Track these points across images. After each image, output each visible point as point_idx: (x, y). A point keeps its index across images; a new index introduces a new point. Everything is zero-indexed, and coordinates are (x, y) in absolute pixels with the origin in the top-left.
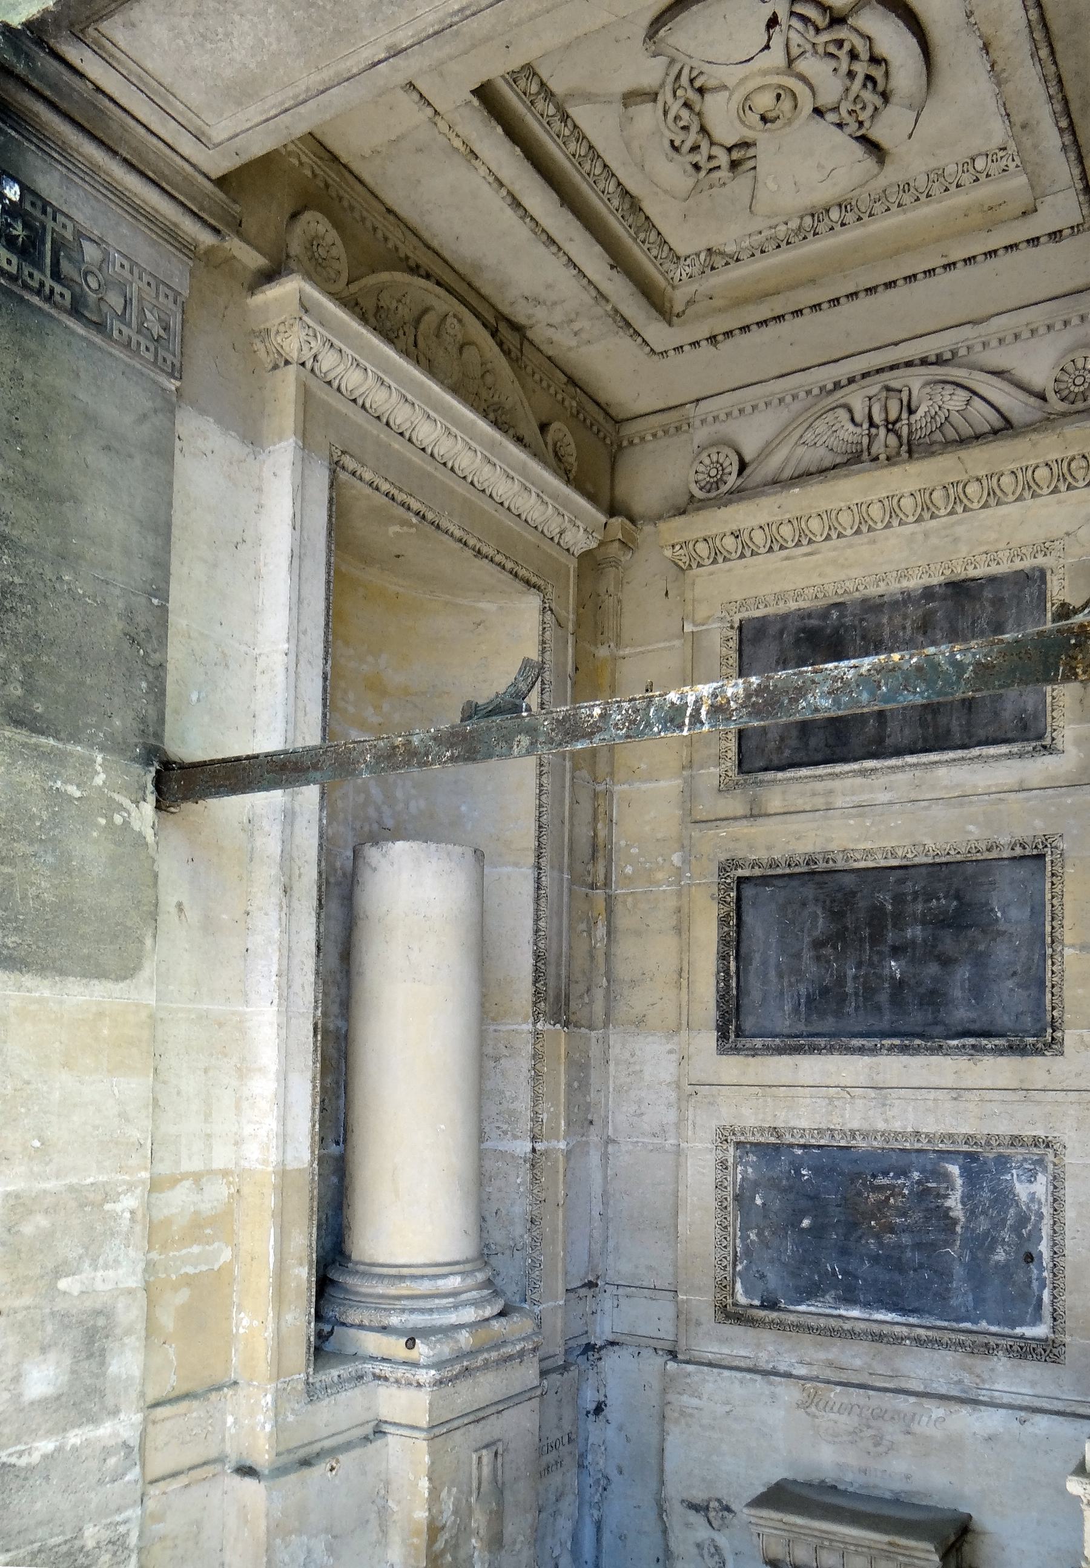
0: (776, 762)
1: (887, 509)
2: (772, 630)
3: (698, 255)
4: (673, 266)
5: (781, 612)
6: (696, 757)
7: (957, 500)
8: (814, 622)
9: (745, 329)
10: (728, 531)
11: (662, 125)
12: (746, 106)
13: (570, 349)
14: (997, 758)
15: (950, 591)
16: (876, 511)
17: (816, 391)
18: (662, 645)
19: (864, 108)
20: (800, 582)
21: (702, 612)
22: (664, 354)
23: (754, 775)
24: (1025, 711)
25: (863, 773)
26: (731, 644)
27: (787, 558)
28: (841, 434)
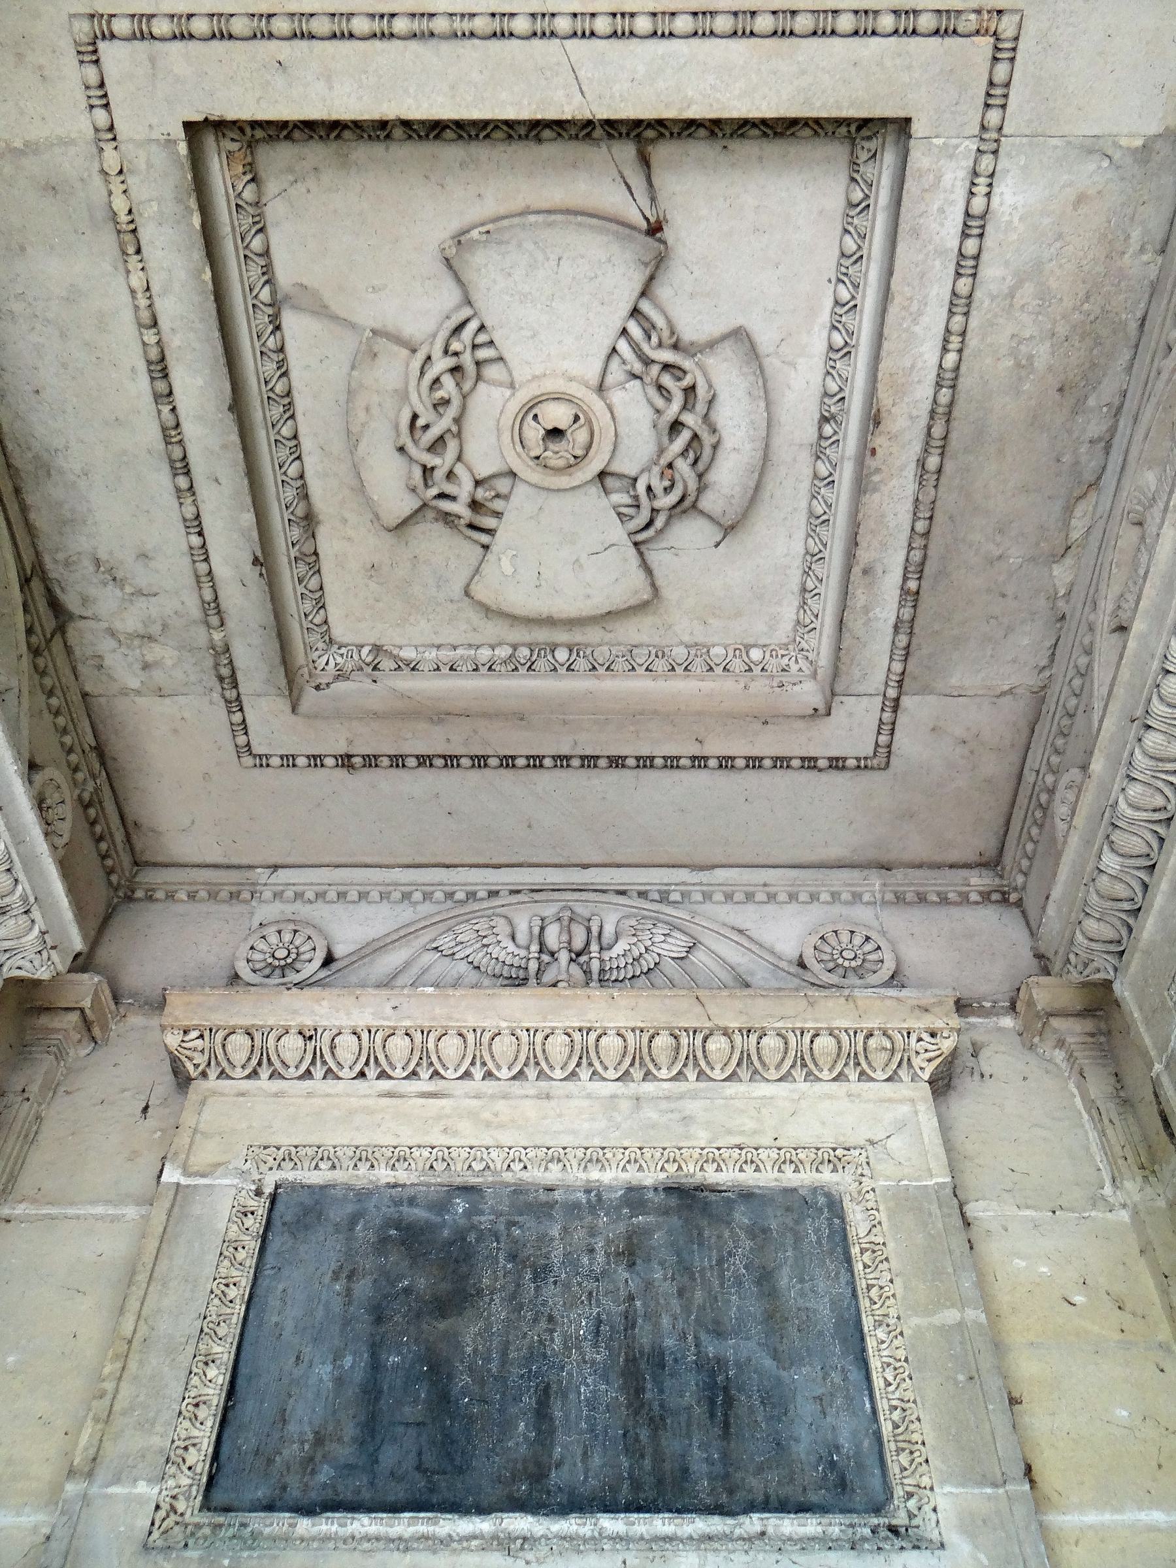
0: (294, 1493)
1: (578, 1047)
2: (337, 1214)
3: (360, 647)
4: (321, 645)
5: (359, 1184)
6: (111, 1450)
7: (691, 1058)
8: (419, 1213)
9: (398, 761)
10: (294, 1022)
11: (413, 383)
12: (530, 410)
13: (125, 692)
14: (805, 1544)
15: (673, 1201)
16: (558, 1046)
17: (460, 896)
18: (99, 1210)
19: (667, 490)
20: (408, 1137)
21: (205, 1154)
22: (263, 762)
23: (242, 1517)
24: (837, 1448)
25: (505, 1544)
26: (249, 1221)
27: (390, 1095)
28: (495, 951)
